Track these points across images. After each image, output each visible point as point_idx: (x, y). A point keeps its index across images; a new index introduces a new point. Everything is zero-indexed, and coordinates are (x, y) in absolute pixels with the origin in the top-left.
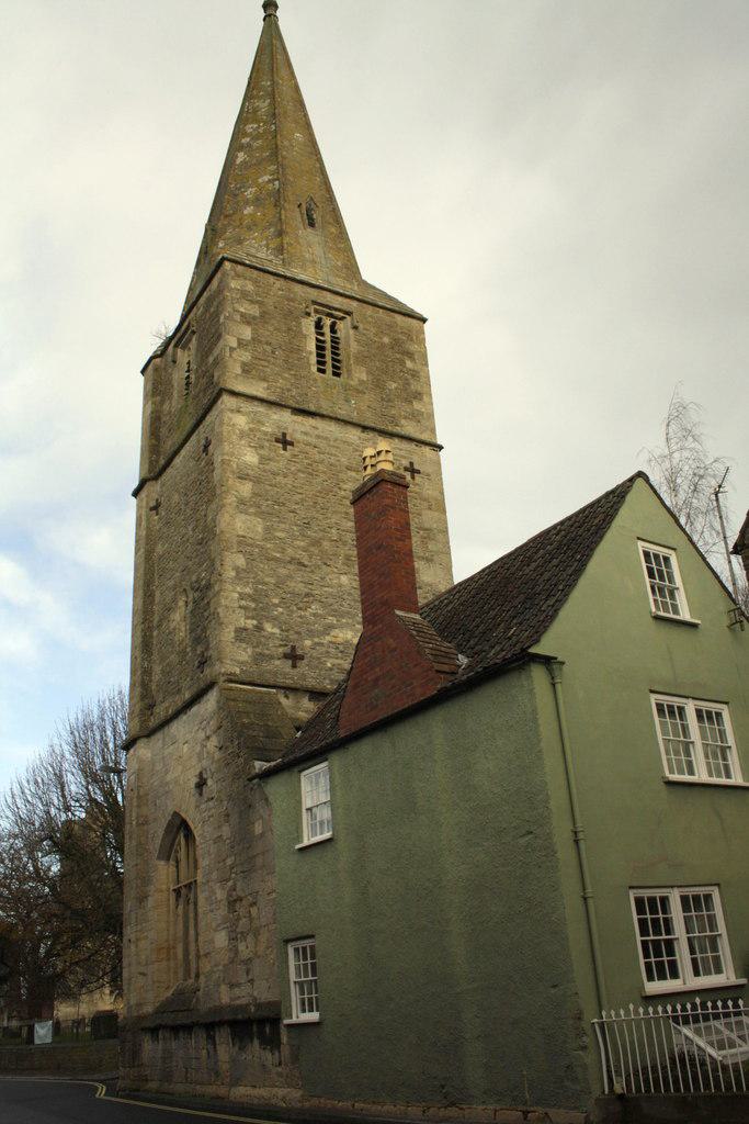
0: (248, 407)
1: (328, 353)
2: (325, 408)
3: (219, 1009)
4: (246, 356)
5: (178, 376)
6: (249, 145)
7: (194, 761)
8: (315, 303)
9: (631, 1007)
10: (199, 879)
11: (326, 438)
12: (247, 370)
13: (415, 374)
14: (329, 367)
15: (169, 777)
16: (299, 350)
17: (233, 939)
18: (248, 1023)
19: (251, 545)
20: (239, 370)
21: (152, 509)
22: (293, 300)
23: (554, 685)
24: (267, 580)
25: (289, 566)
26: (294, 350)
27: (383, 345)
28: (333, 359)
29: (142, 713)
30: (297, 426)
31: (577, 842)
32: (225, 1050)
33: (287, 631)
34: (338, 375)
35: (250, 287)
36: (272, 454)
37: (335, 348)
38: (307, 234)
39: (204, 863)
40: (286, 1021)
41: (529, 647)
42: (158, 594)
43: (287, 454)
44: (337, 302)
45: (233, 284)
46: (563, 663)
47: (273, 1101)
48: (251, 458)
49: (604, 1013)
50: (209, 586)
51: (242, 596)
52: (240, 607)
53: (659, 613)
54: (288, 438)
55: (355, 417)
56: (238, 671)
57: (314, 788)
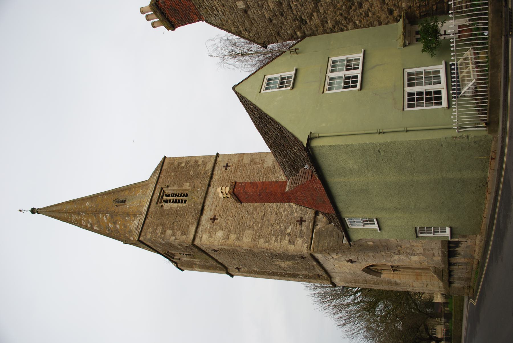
0: (199, 234)
1: (178, 198)
2: (200, 201)
3: (443, 261)
4: (179, 233)
5: (185, 259)
6: (91, 224)
7: (342, 263)
8: (157, 203)
9: (452, 117)
10: (390, 264)
11: (213, 202)
12: (184, 233)
13: (187, 163)
14: (184, 198)
15: (347, 271)
16: (176, 211)
17: (415, 254)
18: (449, 252)
19: (256, 236)
20: (184, 237)
21: (239, 271)
22: (156, 212)
23: (319, 137)
24: (269, 230)
25: (264, 220)
26: (176, 212)
27: (176, 176)
28: (180, 196)
29: (322, 279)
30: (207, 215)
31: (384, 133)
32: (459, 260)
33: (290, 223)
34: (187, 195)
35: (150, 230)
36: (219, 225)
37: (176, 195)
38: (128, 204)
39: (383, 262)
40: (449, 239)
41: (303, 146)
42: (273, 271)
43: (219, 219)
44: (157, 194)
45: (149, 237)
46: (311, 133)
47: (481, 245)
48: (220, 234)
49: (454, 128)
50: (271, 253)
51: (276, 241)
52: (280, 242)
53: (291, 86)
54: (213, 218)
55: (204, 189)
56: (306, 245)
57: (356, 226)
